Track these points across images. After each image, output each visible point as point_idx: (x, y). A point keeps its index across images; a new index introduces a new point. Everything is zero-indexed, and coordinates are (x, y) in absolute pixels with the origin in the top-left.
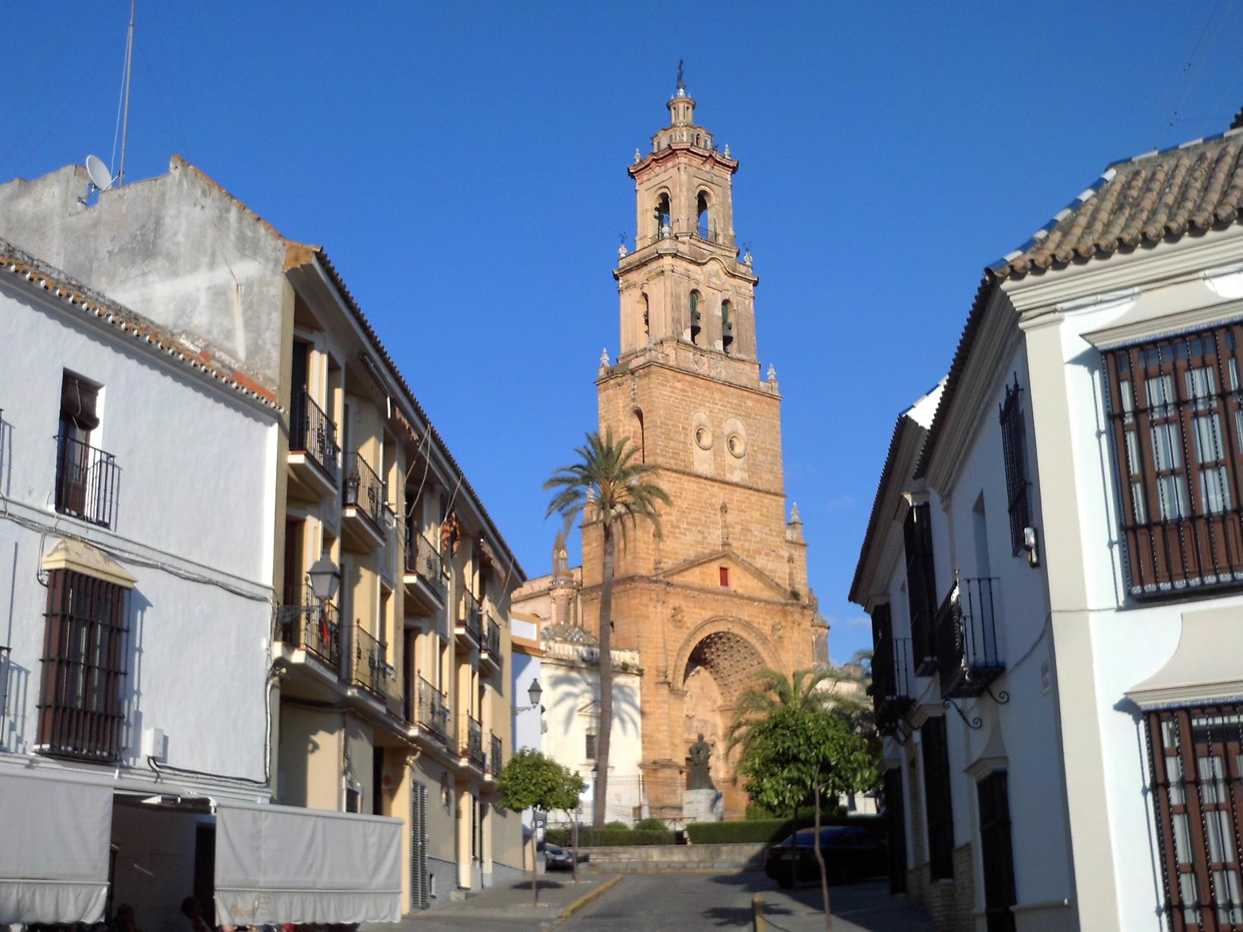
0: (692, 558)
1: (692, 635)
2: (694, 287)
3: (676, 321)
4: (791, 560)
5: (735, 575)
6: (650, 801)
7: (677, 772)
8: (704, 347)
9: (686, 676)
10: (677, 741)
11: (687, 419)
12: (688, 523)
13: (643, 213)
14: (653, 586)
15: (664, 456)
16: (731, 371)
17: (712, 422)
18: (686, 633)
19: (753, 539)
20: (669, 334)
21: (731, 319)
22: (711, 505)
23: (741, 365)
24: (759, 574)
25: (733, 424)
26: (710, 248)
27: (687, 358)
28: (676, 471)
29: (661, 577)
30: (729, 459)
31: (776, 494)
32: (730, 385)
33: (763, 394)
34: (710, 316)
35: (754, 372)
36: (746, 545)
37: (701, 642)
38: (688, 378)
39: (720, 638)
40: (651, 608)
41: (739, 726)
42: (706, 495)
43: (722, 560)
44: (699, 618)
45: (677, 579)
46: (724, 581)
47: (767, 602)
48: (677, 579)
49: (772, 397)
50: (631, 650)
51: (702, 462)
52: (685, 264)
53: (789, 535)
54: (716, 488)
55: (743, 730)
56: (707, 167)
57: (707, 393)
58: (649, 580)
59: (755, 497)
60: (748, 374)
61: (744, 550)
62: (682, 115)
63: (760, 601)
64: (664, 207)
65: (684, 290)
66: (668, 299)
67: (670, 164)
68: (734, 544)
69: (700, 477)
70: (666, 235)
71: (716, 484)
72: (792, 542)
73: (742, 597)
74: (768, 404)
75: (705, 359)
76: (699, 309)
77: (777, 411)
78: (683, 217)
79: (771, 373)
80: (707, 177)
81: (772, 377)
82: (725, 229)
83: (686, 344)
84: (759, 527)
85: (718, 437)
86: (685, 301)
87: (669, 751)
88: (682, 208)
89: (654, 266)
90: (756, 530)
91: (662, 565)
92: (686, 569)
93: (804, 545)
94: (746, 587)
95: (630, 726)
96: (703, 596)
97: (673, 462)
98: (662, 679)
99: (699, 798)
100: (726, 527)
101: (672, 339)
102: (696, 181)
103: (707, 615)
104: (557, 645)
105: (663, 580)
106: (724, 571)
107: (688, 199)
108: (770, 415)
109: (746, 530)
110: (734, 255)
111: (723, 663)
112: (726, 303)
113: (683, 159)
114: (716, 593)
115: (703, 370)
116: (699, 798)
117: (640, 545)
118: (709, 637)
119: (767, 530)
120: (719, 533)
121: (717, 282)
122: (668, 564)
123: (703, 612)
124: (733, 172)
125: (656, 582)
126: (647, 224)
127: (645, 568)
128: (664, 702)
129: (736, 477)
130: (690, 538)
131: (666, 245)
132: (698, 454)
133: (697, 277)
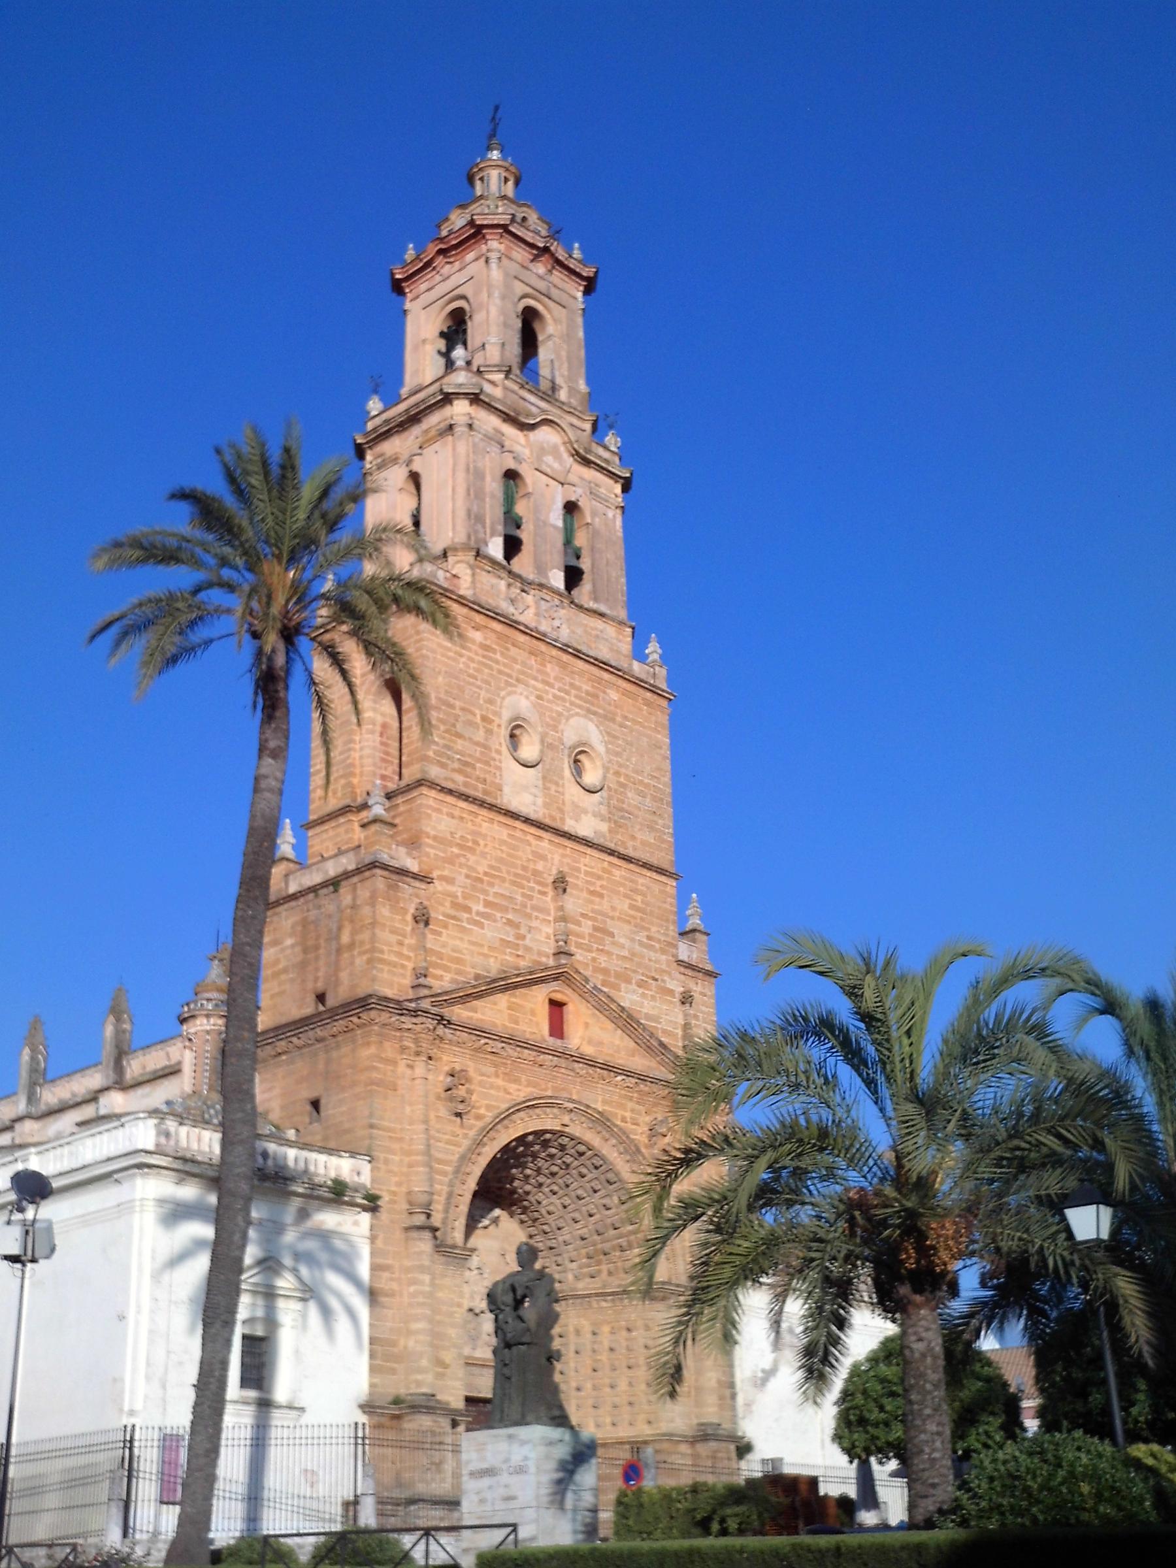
0: (493, 974)
1: (489, 1130)
2: (512, 465)
3: (475, 518)
4: (686, 999)
5: (578, 1014)
6: (378, 1483)
7: (445, 1423)
8: (531, 577)
9: (471, 1227)
10: (448, 1356)
11: (491, 702)
12: (488, 904)
13: (416, 348)
14: (408, 1022)
15: (443, 766)
16: (579, 631)
17: (542, 715)
18: (474, 1125)
19: (616, 951)
20: (461, 538)
21: (581, 540)
22: (536, 873)
23: (598, 623)
24: (627, 1021)
25: (581, 728)
26: (543, 404)
27: (495, 589)
28: (465, 797)
29: (425, 1004)
30: (573, 792)
31: (661, 871)
32: (577, 654)
33: (638, 682)
34: (541, 524)
35: (625, 642)
36: (603, 960)
37: (506, 1149)
38: (495, 625)
39: (545, 1144)
40: (402, 1068)
41: (690, 1158)
42: (525, 853)
43: (554, 986)
44: (503, 1098)
45: (458, 1013)
46: (557, 1028)
47: (642, 1078)
48: (458, 1013)
49: (654, 690)
50: (353, 1154)
51: (520, 790)
52: (494, 421)
53: (685, 951)
54: (546, 844)
55: (712, 1173)
56: (540, 268)
57: (532, 661)
58: (400, 1008)
59: (621, 871)
60: (613, 641)
61: (597, 970)
62: (495, 179)
63: (628, 1073)
64: (456, 329)
65: (493, 465)
66: (461, 475)
67: (470, 256)
68: (580, 956)
69: (514, 816)
70: (460, 363)
71: (546, 835)
72: (689, 966)
73: (591, 1063)
74: (648, 703)
75: (529, 599)
76: (520, 508)
77: (664, 719)
78: (493, 340)
79: (653, 649)
80: (541, 285)
81: (656, 656)
82: (570, 379)
83: (493, 562)
84: (626, 927)
85: (551, 746)
86: (494, 486)
87: (429, 1378)
88: (493, 334)
89: (434, 420)
90: (622, 933)
91: (429, 981)
92: (479, 996)
93: (709, 974)
94: (601, 1043)
95: (342, 1324)
96: (510, 1051)
97: (460, 778)
98: (420, 1220)
99: (518, 1454)
100: (564, 919)
101: (466, 547)
102: (520, 288)
103: (520, 1092)
104: (184, 1130)
105: (430, 1011)
106: (556, 1006)
107: (502, 312)
108: (651, 726)
109: (602, 931)
110: (588, 426)
111: (547, 1202)
112: (571, 508)
113: (495, 244)
114: (540, 1049)
115: (527, 617)
116: (518, 1454)
117: (384, 935)
118: (521, 1140)
119: (642, 936)
120: (549, 930)
121: (558, 468)
122: (442, 981)
123: (512, 1087)
124: (588, 291)
125: (415, 1013)
126: (422, 364)
127: (393, 982)
128: (422, 1269)
129: (586, 827)
130: (491, 932)
131: (460, 379)
132: (512, 773)
133: (518, 448)
